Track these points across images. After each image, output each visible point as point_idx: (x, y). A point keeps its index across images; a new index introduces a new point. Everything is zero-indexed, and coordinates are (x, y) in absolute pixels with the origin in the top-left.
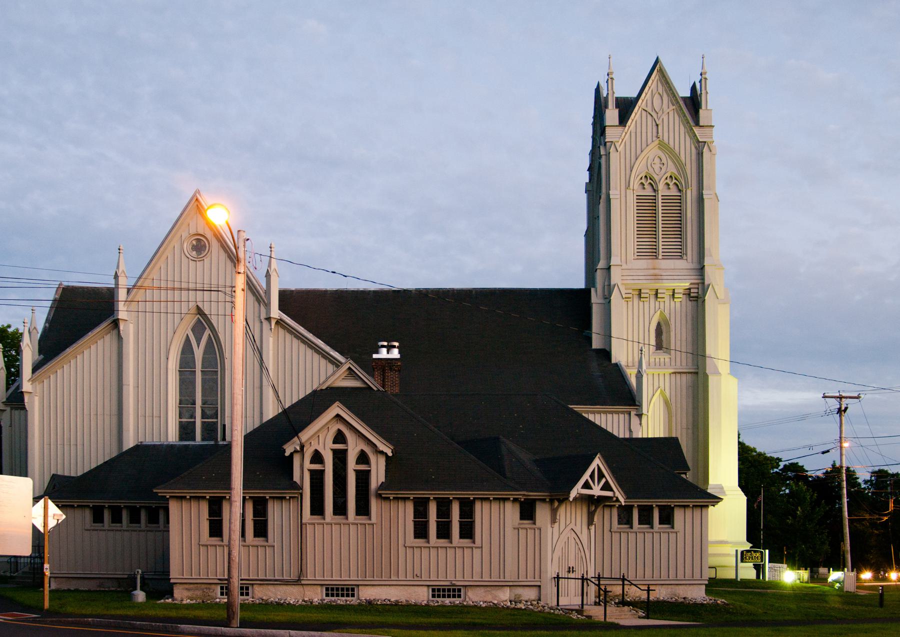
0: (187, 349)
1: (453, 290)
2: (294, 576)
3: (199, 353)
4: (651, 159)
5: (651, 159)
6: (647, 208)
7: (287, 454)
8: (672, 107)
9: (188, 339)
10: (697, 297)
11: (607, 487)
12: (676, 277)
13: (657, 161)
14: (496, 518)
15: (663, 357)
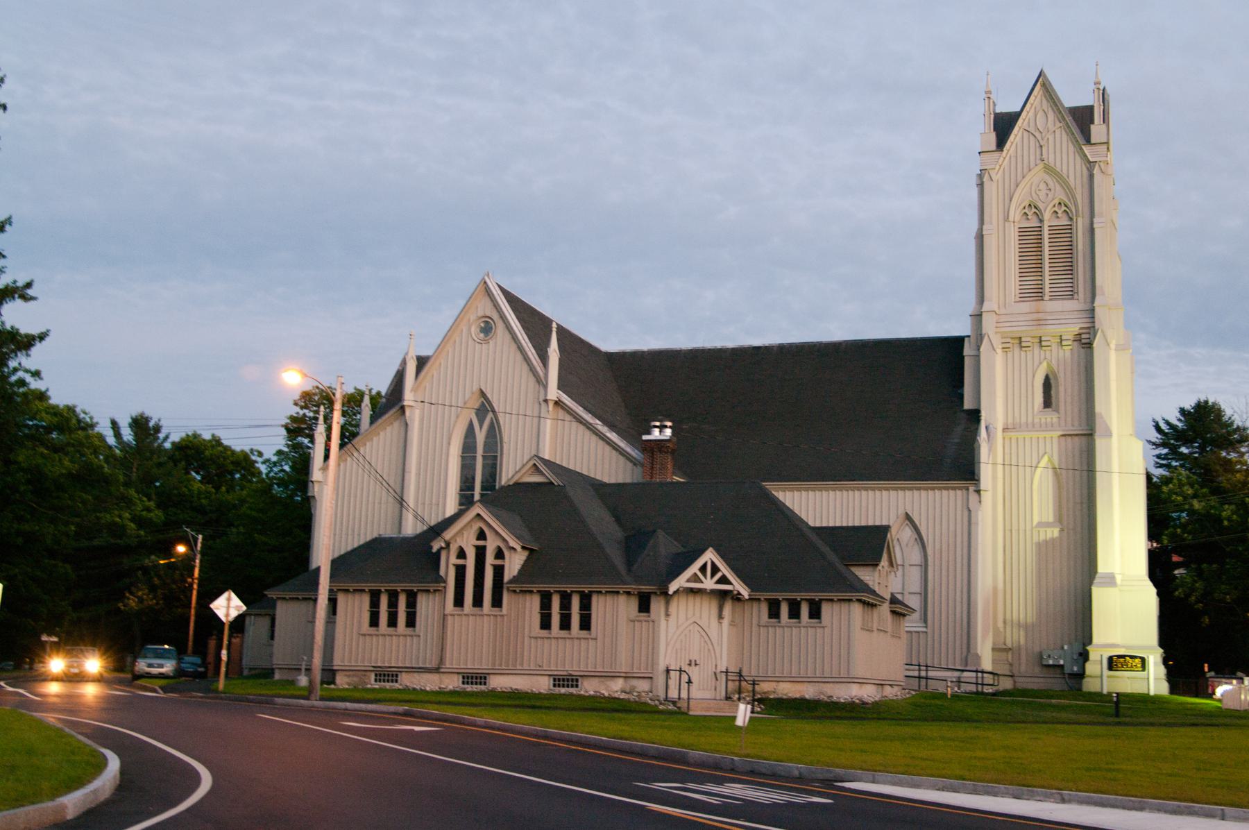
0: (470, 432)
1: (820, 343)
2: (434, 664)
3: (481, 436)
4: (1034, 185)
5: (1034, 185)
6: (1031, 241)
7: (435, 550)
8: (1059, 125)
9: (471, 425)
10: (1086, 342)
11: (724, 580)
12: (1063, 318)
13: (1042, 186)
14: (614, 612)
15: (1050, 417)
